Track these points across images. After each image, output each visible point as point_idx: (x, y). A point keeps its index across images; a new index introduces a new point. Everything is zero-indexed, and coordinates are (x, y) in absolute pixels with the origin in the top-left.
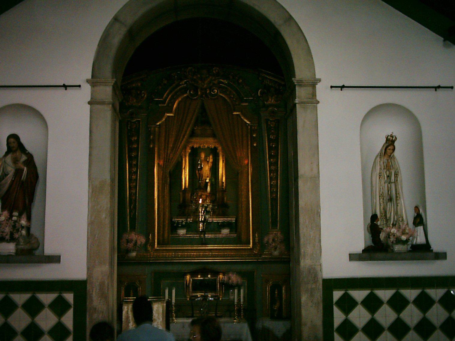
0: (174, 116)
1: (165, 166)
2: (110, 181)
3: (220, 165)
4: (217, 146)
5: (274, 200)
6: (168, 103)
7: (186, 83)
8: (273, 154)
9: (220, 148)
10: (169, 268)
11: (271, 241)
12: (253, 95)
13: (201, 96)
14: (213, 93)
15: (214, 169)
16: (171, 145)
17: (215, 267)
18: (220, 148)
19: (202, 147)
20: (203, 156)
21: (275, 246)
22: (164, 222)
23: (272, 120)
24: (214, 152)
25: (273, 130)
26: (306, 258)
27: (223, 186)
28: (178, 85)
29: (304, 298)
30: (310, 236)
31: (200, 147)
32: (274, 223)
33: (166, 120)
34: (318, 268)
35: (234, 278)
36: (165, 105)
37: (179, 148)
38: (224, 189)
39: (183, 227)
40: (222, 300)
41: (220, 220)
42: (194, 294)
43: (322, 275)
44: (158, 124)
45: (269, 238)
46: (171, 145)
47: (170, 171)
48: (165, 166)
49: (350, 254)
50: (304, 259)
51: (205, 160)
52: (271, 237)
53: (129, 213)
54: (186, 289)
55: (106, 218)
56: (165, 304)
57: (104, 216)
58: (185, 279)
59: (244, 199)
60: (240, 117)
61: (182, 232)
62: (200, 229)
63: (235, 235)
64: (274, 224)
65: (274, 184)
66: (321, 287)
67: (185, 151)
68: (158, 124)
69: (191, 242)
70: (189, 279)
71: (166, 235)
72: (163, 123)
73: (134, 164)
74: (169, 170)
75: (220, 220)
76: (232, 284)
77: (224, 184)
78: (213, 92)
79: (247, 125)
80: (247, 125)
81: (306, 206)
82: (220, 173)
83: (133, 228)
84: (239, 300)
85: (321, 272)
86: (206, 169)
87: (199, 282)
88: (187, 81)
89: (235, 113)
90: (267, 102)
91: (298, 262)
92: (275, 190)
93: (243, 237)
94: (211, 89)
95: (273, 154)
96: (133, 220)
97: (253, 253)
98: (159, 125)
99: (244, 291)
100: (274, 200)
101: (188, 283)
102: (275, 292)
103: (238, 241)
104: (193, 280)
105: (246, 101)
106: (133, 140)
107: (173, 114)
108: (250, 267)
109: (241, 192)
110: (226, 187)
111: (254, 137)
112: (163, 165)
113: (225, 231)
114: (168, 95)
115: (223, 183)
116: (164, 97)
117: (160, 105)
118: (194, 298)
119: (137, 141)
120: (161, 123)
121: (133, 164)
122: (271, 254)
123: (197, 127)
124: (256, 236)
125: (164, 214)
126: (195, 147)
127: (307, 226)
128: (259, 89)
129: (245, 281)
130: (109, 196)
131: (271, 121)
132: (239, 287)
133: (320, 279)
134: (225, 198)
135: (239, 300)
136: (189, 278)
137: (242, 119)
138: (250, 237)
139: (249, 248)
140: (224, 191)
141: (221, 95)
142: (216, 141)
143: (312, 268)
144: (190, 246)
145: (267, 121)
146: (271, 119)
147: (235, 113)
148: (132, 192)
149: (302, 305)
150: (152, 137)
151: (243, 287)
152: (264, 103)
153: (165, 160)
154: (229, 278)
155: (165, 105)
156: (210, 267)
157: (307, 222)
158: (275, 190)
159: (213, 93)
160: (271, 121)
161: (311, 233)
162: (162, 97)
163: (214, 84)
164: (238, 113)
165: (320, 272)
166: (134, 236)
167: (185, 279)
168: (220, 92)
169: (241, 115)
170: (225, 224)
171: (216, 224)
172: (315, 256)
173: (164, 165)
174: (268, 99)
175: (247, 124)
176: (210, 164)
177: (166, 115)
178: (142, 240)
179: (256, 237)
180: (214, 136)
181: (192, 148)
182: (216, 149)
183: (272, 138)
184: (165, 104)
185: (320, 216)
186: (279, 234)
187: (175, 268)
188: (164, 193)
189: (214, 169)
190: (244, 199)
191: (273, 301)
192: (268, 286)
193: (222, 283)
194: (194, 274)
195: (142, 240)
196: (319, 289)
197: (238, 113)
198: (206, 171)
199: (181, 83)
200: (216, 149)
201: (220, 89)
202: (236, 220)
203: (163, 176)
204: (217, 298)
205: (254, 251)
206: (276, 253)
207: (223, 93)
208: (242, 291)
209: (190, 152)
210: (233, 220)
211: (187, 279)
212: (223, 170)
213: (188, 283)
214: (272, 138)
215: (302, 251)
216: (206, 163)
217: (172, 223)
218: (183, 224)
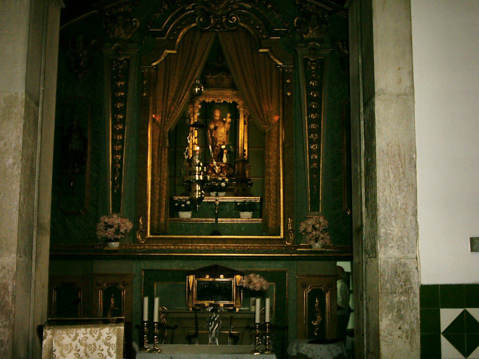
0: (177, 54)
1: (163, 123)
2: (24, 97)
3: (240, 126)
4: (236, 100)
5: (315, 171)
6: (169, 36)
7: (193, 8)
8: (314, 106)
9: (241, 103)
10: (166, 265)
11: (309, 230)
12: (286, 26)
13: (215, 27)
14: (231, 22)
15: (233, 132)
16: (172, 94)
17: (231, 265)
18: (241, 103)
19: (216, 102)
20: (217, 114)
21: (316, 235)
22: (160, 201)
23: (312, 60)
24: (233, 109)
25: (314, 74)
26: (390, 245)
27: (245, 155)
28: (183, 11)
29: (385, 323)
30: (397, 203)
31: (213, 102)
32: (315, 206)
33: (165, 59)
34: (412, 266)
35: (258, 282)
36: (165, 38)
37: (183, 97)
38: (246, 159)
39: (187, 209)
40: (240, 310)
41: (240, 199)
42: (200, 302)
43: (419, 277)
44: (155, 64)
45: (307, 225)
46: (172, 94)
47: (170, 130)
48: (163, 123)
49: (472, 240)
50: (386, 246)
51: (221, 119)
52: (310, 222)
53: (112, 186)
54: (188, 296)
55: (14, 164)
56: (122, 328)
57: (11, 161)
58: (187, 280)
59: (272, 188)
60: (269, 57)
61: (186, 215)
62: (197, 194)
63: (260, 219)
64: (315, 206)
65: (315, 148)
66: (417, 300)
67: (194, 107)
68: (155, 64)
69: (198, 229)
70: (192, 281)
71: (162, 220)
72: (161, 62)
73: (121, 118)
74: (169, 129)
75: (240, 199)
76: (255, 289)
77: (246, 153)
78: (232, 21)
79: (279, 67)
80: (279, 67)
81: (389, 148)
82: (240, 143)
83: (117, 209)
84: (263, 314)
85: (418, 272)
86: (222, 132)
87: (207, 285)
88: (196, 5)
89: (261, 50)
90: (306, 35)
91: (373, 253)
92: (316, 158)
93: (271, 223)
94: (229, 17)
95: (314, 106)
96: (117, 197)
97: (285, 245)
98: (157, 65)
99: (271, 302)
100: (315, 171)
101: (191, 286)
102: (316, 300)
103: (264, 229)
104: (198, 281)
105: (277, 34)
106: (119, 85)
107: (176, 51)
108: (278, 266)
109: (269, 176)
110: (248, 156)
111: (288, 83)
112: (160, 121)
113: (246, 216)
114: (169, 24)
115: (245, 151)
116: (163, 28)
117: (157, 38)
118: (199, 308)
119: (125, 88)
120: (159, 64)
121: (118, 118)
122: (310, 247)
123: (210, 74)
124: (289, 221)
125: (161, 189)
126: (207, 102)
127: (390, 185)
128: (296, 17)
129: (272, 284)
130: (21, 125)
131: (311, 61)
132: (262, 294)
133: (416, 285)
134: (247, 172)
135: (263, 314)
136: (192, 279)
137: (271, 58)
138: (280, 221)
139: (279, 237)
140: (245, 162)
141: (242, 25)
142: (235, 92)
143: (401, 264)
144: (307, 305)
145: (305, 61)
146: (311, 59)
147: (261, 50)
148: (116, 158)
149: (382, 333)
150: (145, 82)
151: (303, 34)
152: (302, 37)
153: (164, 114)
154: (250, 282)
155: (165, 38)
156: (223, 264)
157: (392, 178)
158: (316, 158)
159: (231, 22)
160: (311, 61)
161: (398, 197)
162: (160, 28)
163: (233, 10)
164: (265, 50)
165: (416, 271)
166: (115, 220)
167: (187, 280)
168: (242, 22)
169: (270, 54)
170: (246, 204)
171: (234, 204)
172: (406, 240)
173: (161, 121)
174: (308, 31)
175: (278, 65)
176: (227, 126)
177: (166, 52)
178: (128, 225)
179: (289, 222)
180: (233, 87)
181: (204, 103)
182: (235, 104)
183: (313, 84)
184: (165, 37)
185: (415, 166)
186: (321, 219)
187: (175, 266)
188: (161, 161)
189: (233, 132)
190: (272, 188)
191: (312, 316)
192: (306, 292)
193: (240, 288)
194: (199, 273)
195: (128, 225)
196: (413, 304)
197: (265, 50)
198: (222, 133)
199: (187, 8)
200: (235, 104)
201: (241, 17)
202: (261, 200)
203: (160, 136)
204: (232, 308)
205: (286, 243)
206: (317, 246)
207: (245, 23)
208: (268, 301)
209: (200, 107)
210: (257, 199)
211: (189, 280)
212: (245, 134)
213: (191, 286)
214: (313, 84)
215: (383, 230)
216: (222, 124)
217: (171, 201)
218: (187, 204)
